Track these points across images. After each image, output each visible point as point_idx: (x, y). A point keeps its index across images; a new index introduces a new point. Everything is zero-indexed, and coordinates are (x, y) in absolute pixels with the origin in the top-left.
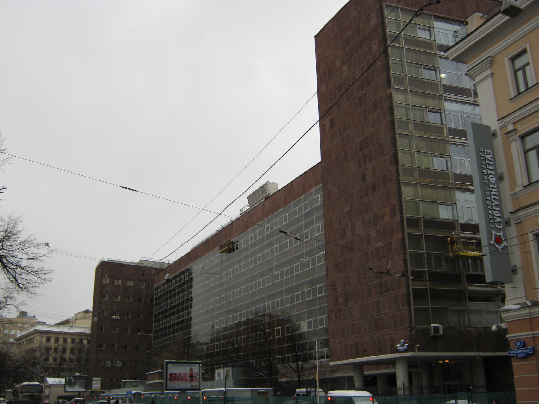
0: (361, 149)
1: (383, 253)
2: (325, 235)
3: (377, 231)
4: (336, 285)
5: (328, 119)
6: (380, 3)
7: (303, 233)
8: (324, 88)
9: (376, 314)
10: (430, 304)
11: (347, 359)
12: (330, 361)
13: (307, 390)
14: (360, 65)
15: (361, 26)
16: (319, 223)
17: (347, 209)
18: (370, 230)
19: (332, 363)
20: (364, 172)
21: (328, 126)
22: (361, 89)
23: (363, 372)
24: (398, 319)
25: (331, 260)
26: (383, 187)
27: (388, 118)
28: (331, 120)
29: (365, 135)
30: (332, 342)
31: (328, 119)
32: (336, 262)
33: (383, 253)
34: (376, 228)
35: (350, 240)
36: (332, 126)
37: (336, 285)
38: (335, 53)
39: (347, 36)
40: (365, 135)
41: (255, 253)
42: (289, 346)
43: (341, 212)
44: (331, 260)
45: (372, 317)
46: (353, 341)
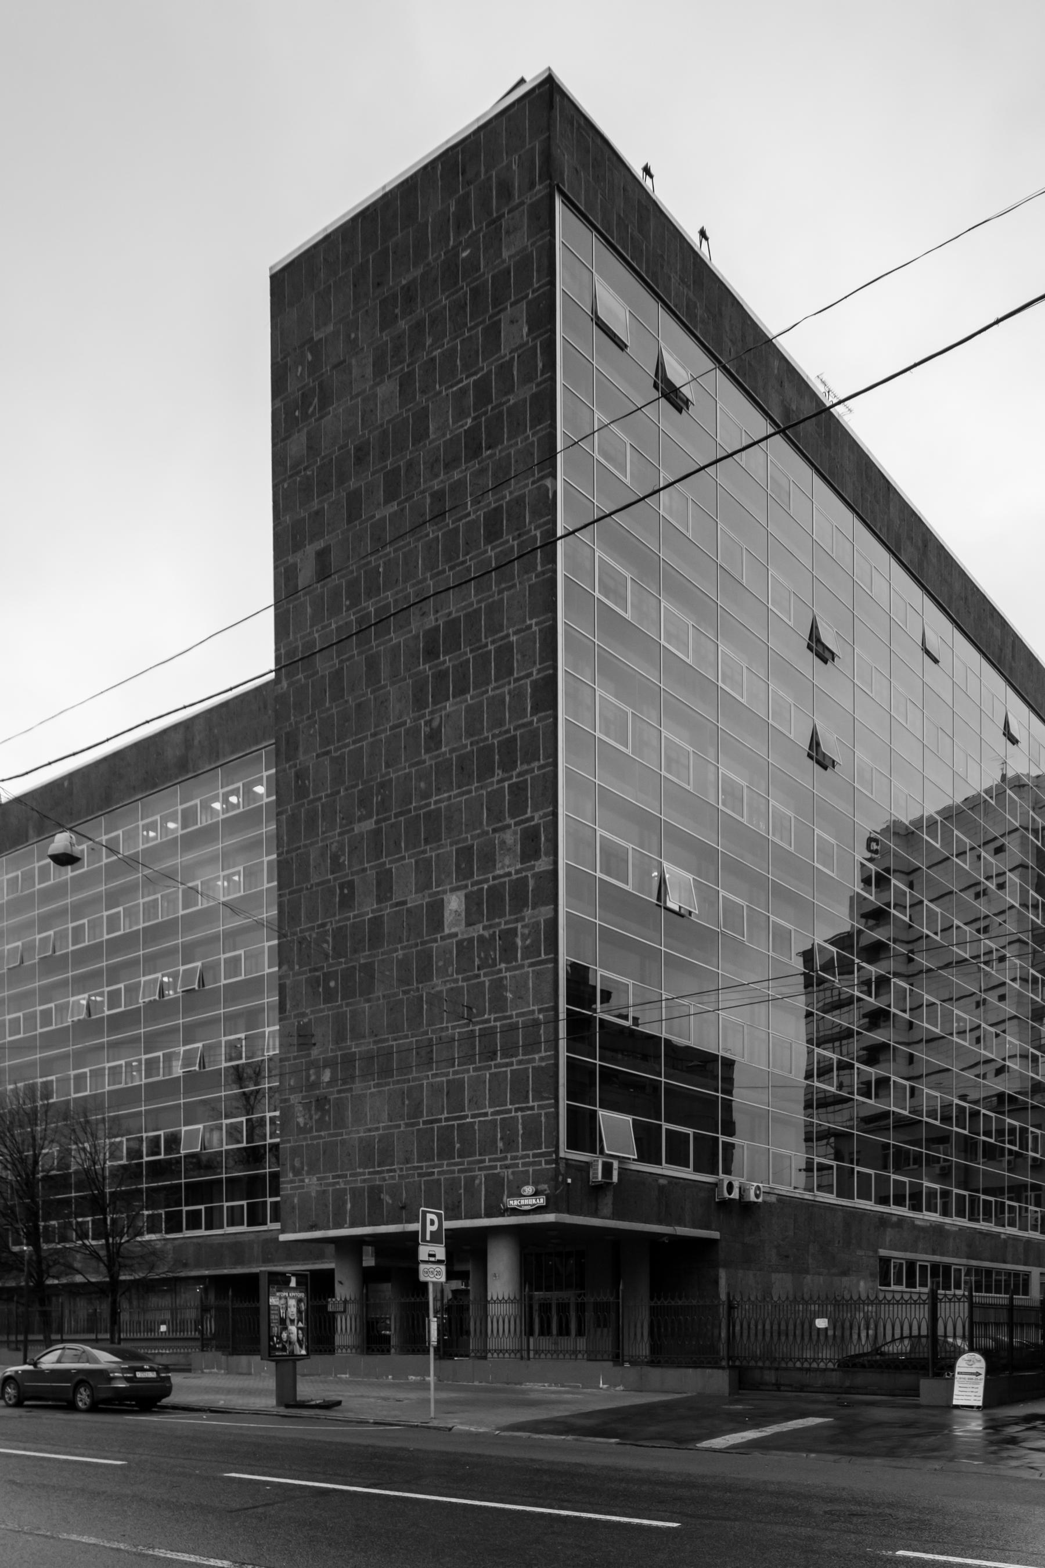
0: (431, 653)
1: (482, 955)
2: (280, 896)
3: (467, 896)
4: (313, 1036)
5: (311, 549)
6: (548, 182)
7: (138, 905)
8: (298, 444)
9: (446, 1115)
10: (771, 950)
11: (339, 1225)
12: (283, 1231)
13: (1011, 1299)
14: (452, 386)
15: (465, 254)
16: (155, 894)
17: (369, 825)
18: (444, 892)
19: (283, 1237)
20: (435, 724)
21: (306, 574)
22: (446, 466)
23: (361, 1261)
24: (521, 1132)
25: (297, 967)
26: (500, 772)
27: (539, 568)
28: (322, 555)
29: (450, 614)
30: (292, 1182)
31: (311, 549)
32: (317, 974)
33: (482, 955)
34: (494, 878)
35: (370, 916)
36: (323, 573)
37: (313, 1036)
38: (353, 336)
39: (404, 282)
40: (450, 614)
41: (78, 911)
42: (81, 1197)
43: (340, 834)
44: (297, 967)
45: (432, 1122)
46: (364, 1181)
